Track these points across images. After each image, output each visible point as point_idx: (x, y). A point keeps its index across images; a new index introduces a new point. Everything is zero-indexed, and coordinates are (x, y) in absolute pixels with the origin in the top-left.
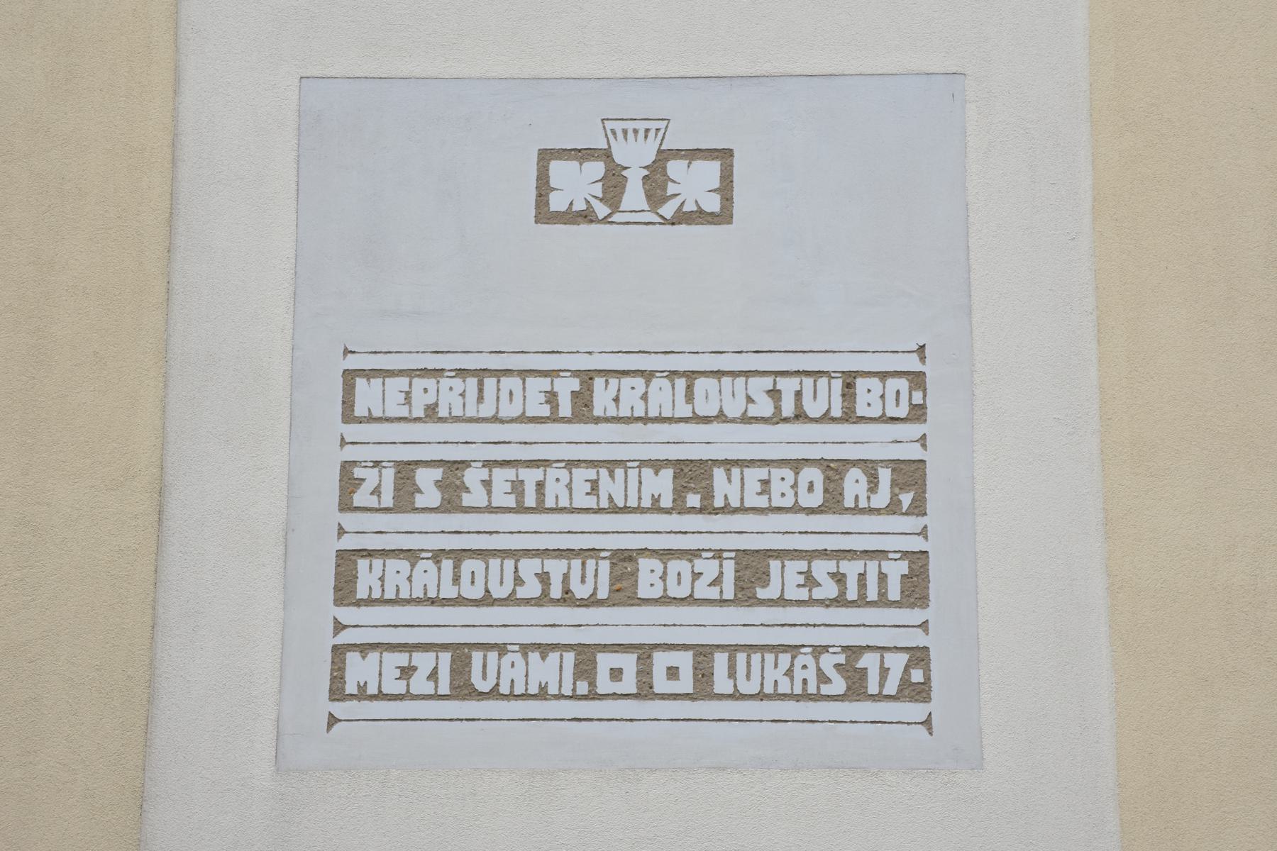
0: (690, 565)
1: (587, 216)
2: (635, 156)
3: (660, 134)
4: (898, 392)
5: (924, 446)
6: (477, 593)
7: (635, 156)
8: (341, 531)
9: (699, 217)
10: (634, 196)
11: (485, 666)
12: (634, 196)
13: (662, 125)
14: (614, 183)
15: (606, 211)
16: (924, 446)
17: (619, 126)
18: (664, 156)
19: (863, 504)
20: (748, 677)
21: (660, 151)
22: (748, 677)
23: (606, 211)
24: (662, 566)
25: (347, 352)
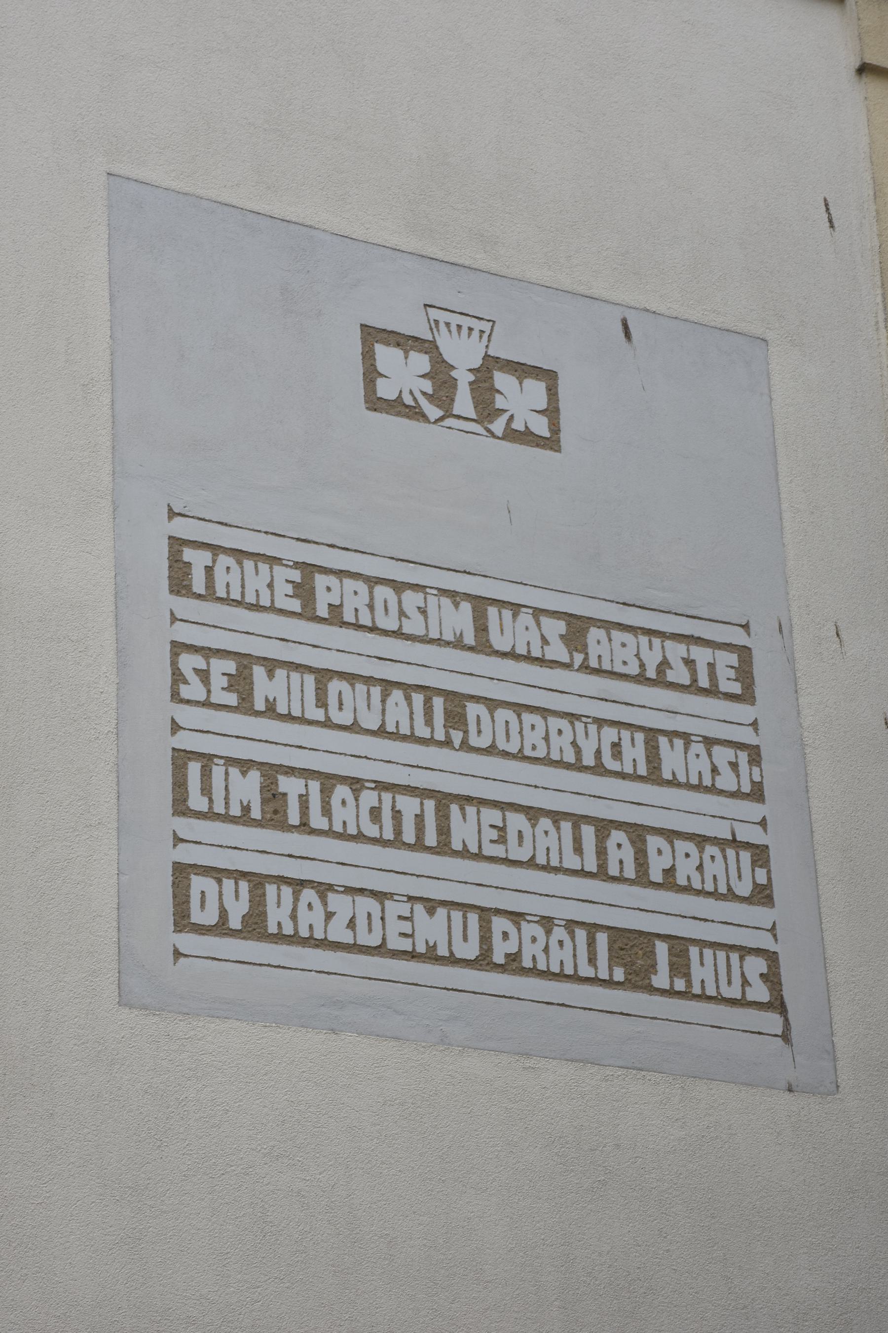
0: (504, 848)
1: (415, 413)
2: (463, 355)
3: (485, 336)
4: (369, 915)
5: (756, 730)
6: (374, 940)
7: (463, 355)
8: (175, 727)
9: (526, 437)
10: (464, 403)
11: (739, 869)
12: (464, 403)
13: (486, 327)
14: (441, 375)
15: (439, 413)
16: (756, 730)
17: (443, 316)
18: (491, 364)
19: (319, 934)
20: (729, 983)
21: (486, 356)
22: (729, 983)
23: (439, 413)
24: (379, 907)
25: (172, 514)
